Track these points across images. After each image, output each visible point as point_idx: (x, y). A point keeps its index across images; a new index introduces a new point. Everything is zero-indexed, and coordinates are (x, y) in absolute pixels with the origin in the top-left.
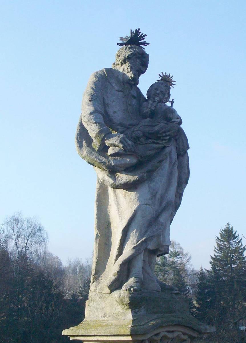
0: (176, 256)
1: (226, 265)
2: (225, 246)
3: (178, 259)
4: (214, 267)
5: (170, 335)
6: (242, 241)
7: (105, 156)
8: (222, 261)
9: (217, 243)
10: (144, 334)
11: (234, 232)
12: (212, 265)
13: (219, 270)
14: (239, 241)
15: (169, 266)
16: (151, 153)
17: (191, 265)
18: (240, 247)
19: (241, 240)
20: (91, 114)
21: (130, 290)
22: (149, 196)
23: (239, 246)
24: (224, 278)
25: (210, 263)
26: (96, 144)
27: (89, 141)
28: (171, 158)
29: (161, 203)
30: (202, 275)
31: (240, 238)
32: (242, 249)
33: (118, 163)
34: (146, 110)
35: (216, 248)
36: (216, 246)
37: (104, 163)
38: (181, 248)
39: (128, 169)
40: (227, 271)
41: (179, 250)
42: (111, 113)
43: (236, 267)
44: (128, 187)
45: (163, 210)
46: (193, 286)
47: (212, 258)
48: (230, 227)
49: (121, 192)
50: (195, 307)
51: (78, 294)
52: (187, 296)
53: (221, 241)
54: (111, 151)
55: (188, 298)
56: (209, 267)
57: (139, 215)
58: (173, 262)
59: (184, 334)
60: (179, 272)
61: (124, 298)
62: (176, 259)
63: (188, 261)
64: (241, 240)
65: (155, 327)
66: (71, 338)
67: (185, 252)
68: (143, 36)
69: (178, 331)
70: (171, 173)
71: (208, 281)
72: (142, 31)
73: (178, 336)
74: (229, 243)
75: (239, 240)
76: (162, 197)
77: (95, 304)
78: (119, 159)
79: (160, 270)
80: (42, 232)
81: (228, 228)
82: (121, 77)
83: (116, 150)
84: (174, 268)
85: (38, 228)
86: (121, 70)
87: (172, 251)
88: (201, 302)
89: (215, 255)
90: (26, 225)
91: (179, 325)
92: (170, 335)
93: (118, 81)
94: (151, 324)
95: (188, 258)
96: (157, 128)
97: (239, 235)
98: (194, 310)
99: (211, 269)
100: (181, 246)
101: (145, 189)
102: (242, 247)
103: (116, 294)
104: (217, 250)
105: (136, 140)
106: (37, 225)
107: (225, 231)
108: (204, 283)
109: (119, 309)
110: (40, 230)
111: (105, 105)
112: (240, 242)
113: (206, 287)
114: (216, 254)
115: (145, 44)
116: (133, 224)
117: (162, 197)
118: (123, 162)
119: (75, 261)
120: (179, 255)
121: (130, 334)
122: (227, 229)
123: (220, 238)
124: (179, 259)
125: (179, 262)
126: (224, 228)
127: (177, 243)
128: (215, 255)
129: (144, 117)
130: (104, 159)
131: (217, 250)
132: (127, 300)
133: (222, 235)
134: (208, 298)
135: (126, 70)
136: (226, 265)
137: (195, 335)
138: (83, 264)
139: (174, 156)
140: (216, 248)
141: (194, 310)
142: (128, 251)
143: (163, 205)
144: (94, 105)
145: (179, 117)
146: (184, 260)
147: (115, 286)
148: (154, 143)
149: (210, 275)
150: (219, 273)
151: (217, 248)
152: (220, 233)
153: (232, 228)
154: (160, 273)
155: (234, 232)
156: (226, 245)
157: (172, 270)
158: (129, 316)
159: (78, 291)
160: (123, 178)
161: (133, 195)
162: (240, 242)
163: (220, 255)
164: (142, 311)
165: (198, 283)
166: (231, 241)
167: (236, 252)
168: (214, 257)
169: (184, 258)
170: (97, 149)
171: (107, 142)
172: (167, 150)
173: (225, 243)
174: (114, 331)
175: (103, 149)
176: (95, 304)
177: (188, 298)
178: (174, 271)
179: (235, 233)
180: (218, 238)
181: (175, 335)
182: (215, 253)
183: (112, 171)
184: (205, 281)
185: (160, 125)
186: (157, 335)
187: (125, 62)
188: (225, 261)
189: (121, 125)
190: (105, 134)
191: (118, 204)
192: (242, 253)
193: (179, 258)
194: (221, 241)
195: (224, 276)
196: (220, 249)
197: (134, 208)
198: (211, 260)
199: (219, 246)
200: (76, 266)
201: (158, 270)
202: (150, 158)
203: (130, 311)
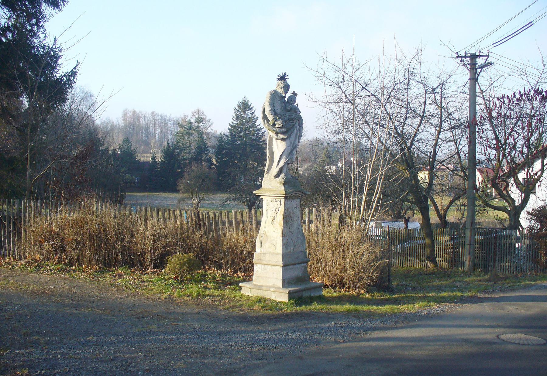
0: (201, 122)
1: (241, 131)
2: (241, 115)
3: (202, 125)
4: (231, 133)
6: (255, 112)
7: (274, 127)
8: (238, 128)
9: (235, 113)
10: (288, 194)
11: (249, 105)
12: (230, 131)
13: (235, 135)
14: (253, 112)
15: (194, 130)
16: (291, 127)
18: (254, 117)
19: (255, 111)
20: (270, 111)
21: (284, 178)
22: (290, 143)
23: (253, 116)
24: (239, 142)
25: (228, 129)
26: (271, 122)
27: (268, 121)
28: (297, 128)
29: (293, 146)
30: (220, 138)
32: (255, 119)
33: (280, 131)
34: (288, 108)
35: (233, 117)
36: (234, 115)
37: (275, 131)
38: (204, 115)
39: (283, 133)
40: (241, 136)
41: (202, 117)
42: (276, 110)
43: (249, 133)
44: (283, 140)
45: (294, 149)
47: (230, 125)
48: (247, 100)
49: (279, 141)
50: (214, 164)
51: (117, 150)
52: (207, 156)
54: (277, 126)
55: (209, 156)
56: (227, 132)
57: (286, 150)
58: (198, 127)
61: (281, 181)
62: (200, 124)
63: (210, 126)
64: (255, 111)
65: (292, 192)
66: (256, 195)
67: (207, 119)
68: (287, 76)
70: (297, 134)
71: (226, 144)
72: (287, 74)
74: (245, 113)
75: (253, 111)
76: (293, 143)
77: (267, 182)
78: (280, 129)
79: (187, 133)
81: (245, 100)
82: (279, 94)
83: (280, 126)
84: (198, 131)
86: (280, 91)
87: (198, 117)
88: (219, 161)
89: (232, 123)
90: (78, 91)
91: (299, 191)
92: (296, 195)
93: (278, 96)
94: (291, 190)
95: (210, 124)
96: (293, 117)
97: (253, 107)
98: (213, 166)
100: (205, 113)
101: (288, 140)
102: (256, 117)
103: (277, 179)
104: (234, 119)
105: (286, 122)
106: (88, 92)
107: (242, 103)
108: (222, 145)
109: (278, 185)
110: (91, 96)
111: (274, 106)
112: (253, 113)
114: (234, 122)
116: (284, 154)
117: (293, 143)
118: (282, 131)
119: (107, 119)
120: (203, 121)
122: (243, 101)
123: (237, 109)
125: (202, 127)
126: (241, 100)
127: (201, 111)
128: (232, 123)
129: (288, 111)
130: (275, 129)
131: (234, 119)
132: (283, 182)
133: (239, 107)
134: (225, 158)
135: (282, 92)
136: (241, 131)
137: (303, 195)
138: (113, 123)
139: (298, 127)
140: (233, 117)
141: (213, 166)
142: (282, 164)
143: (294, 146)
144: (270, 107)
145: (300, 111)
146: (207, 125)
147: (277, 176)
148: (292, 122)
149: (227, 139)
150: (235, 137)
151: (234, 117)
152: (238, 105)
153: (248, 101)
155: (249, 105)
156: (242, 114)
157: (197, 133)
158: (283, 188)
159: (118, 147)
160: (281, 136)
161: (284, 143)
162: (253, 113)
163: (237, 123)
164: (287, 186)
165: (217, 145)
167: (250, 121)
168: (232, 124)
169: (207, 124)
171: (276, 123)
172: (296, 125)
173: (241, 113)
174: (277, 193)
175: (274, 125)
176: (267, 182)
177: (209, 156)
178: (198, 134)
180: (236, 108)
181: (298, 194)
182: (233, 121)
183: (277, 134)
184: (223, 144)
185: (294, 115)
186: (292, 195)
187: (281, 89)
188: (240, 128)
189: (279, 114)
190: (275, 120)
192: (255, 122)
193: (203, 124)
195: (239, 140)
196: (237, 118)
197: (285, 148)
198: (229, 127)
199: (236, 115)
200: (107, 124)
201: (185, 132)
202: (290, 129)
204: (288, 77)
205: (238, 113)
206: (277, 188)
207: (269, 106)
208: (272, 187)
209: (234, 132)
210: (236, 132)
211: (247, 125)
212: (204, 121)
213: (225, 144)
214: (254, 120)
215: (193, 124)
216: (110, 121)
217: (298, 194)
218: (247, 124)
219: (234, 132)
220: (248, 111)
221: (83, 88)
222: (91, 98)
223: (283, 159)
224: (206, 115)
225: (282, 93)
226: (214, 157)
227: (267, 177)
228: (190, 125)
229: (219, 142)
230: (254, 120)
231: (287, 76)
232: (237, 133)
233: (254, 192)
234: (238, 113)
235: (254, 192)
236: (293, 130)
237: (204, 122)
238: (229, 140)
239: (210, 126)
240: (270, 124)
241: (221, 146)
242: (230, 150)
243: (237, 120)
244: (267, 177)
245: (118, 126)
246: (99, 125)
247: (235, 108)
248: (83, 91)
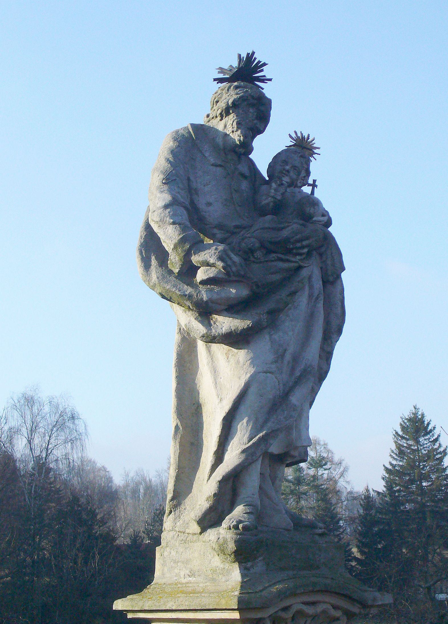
0: (321, 466)
1: (412, 481)
3: (324, 472)
4: (389, 486)
5: (310, 610)
7: (191, 283)
8: (405, 474)
9: (396, 442)
10: (263, 608)
11: (426, 423)
12: (387, 482)
13: (399, 491)
14: (434, 438)
15: (308, 484)
16: (276, 277)
17: (348, 482)
18: (437, 449)
19: (439, 436)
20: (166, 207)
22: (271, 357)
23: (435, 447)
24: (408, 506)
25: (383, 479)
28: (311, 287)
29: (293, 369)
31: (436, 432)
32: (440, 453)
33: (215, 296)
34: (266, 201)
35: (393, 452)
36: (394, 447)
38: (329, 451)
40: (413, 493)
41: (325, 455)
45: (298, 382)
46: (352, 520)
47: (387, 470)
48: (420, 413)
49: (220, 349)
50: (356, 559)
52: (340, 540)
53: (403, 437)
54: (201, 275)
56: (380, 486)
57: (252, 390)
58: (315, 477)
59: (335, 607)
60: (326, 495)
61: (225, 541)
62: (321, 471)
63: (342, 475)
64: (439, 436)
65: (282, 595)
66: (130, 616)
67: (336, 459)
68: (261, 66)
69: (325, 602)
70: (311, 316)
71: (380, 511)
72: (259, 57)
73: (324, 612)
74: (418, 442)
75: (436, 436)
76: (296, 359)
77: (173, 553)
78: (216, 289)
80: (77, 422)
81: (415, 414)
82: (220, 141)
83: (212, 273)
84: (317, 487)
85: (69, 415)
88: (366, 550)
89: (391, 464)
90: (47, 409)
91: (326, 591)
92: (310, 610)
93: (215, 147)
94: (274, 589)
95: (342, 469)
96: (285, 233)
97: (434, 428)
99: (385, 489)
100: (330, 447)
102: (441, 449)
103: (212, 534)
106: (67, 410)
107: (410, 420)
108: (371, 515)
109: (217, 561)
110: (73, 418)
112: (436, 440)
113: (375, 523)
114: (394, 462)
115: (263, 80)
116: (242, 408)
117: (296, 359)
118: (223, 295)
119: (137, 475)
120: (326, 464)
121: (236, 608)
122: (412, 416)
123: (400, 433)
124: (326, 472)
125: (325, 476)
126: (407, 414)
127: (322, 443)
128: (391, 464)
129: (263, 212)
130: (189, 290)
131: (394, 456)
132: (231, 546)
133: (403, 428)
134: (380, 543)
136: (412, 481)
137: (355, 609)
138: (150, 481)
139: (318, 284)
140: (393, 452)
141: (354, 563)
143: (297, 373)
144: (170, 191)
145: (325, 214)
146: (335, 474)
150: (398, 496)
152: (401, 425)
153: (423, 415)
154: (291, 496)
155: (426, 423)
156: (411, 445)
159: (142, 529)
162: (436, 440)
163: (401, 463)
164: (259, 566)
165: (360, 515)
166: (421, 439)
167: (429, 458)
168: (390, 467)
169: (335, 470)
170: (176, 271)
171: (195, 259)
172: (304, 273)
176: (173, 553)
178: (317, 492)
179: (428, 424)
180: (397, 433)
181: (319, 608)
182: (391, 460)
184: (373, 512)
186: (286, 609)
187: (228, 114)
188: (409, 475)
189: (220, 227)
191: (215, 371)
192: (441, 460)
193: (325, 469)
194: (403, 437)
195: (408, 501)
196: (401, 452)
199: (399, 447)
200: (138, 484)
203: (236, 565)
204: (266, 72)
205: (404, 443)
206: (213, 580)
207: (166, 187)
208: (192, 574)
209: (396, 484)
210: (401, 486)
211: (423, 469)
212: (328, 464)
213: (377, 512)
214: (439, 456)
215: (305, 473)
216: (145, 480)
217: (319, 608)
218: (424, 466)
219: (396, 484)
220: (424, 436)
221: (55, 400)
222: (74, 423)
223: (239, 432)
224: (174, 378)
225: (228, 131)
226: (355, 542)
227: (174, 526)
228: (298, 474)
229: (365, 509)
230: (439, 456)
231: (261, 66)
232: (403, 486)
233: (119, 605)
234: (404, 443)
235: (119, 605)
236: (283, 294)
237: (328, 466)
238: (387, 503)
239: (342, 475)
240: (171, 272)
241: (368, 518)
242: (389, 524)
243: (401, 457)
244: (174, 526)
245: (160, 489)
246: (121, 485)
247: (394, 433)
248: (57, 407)
